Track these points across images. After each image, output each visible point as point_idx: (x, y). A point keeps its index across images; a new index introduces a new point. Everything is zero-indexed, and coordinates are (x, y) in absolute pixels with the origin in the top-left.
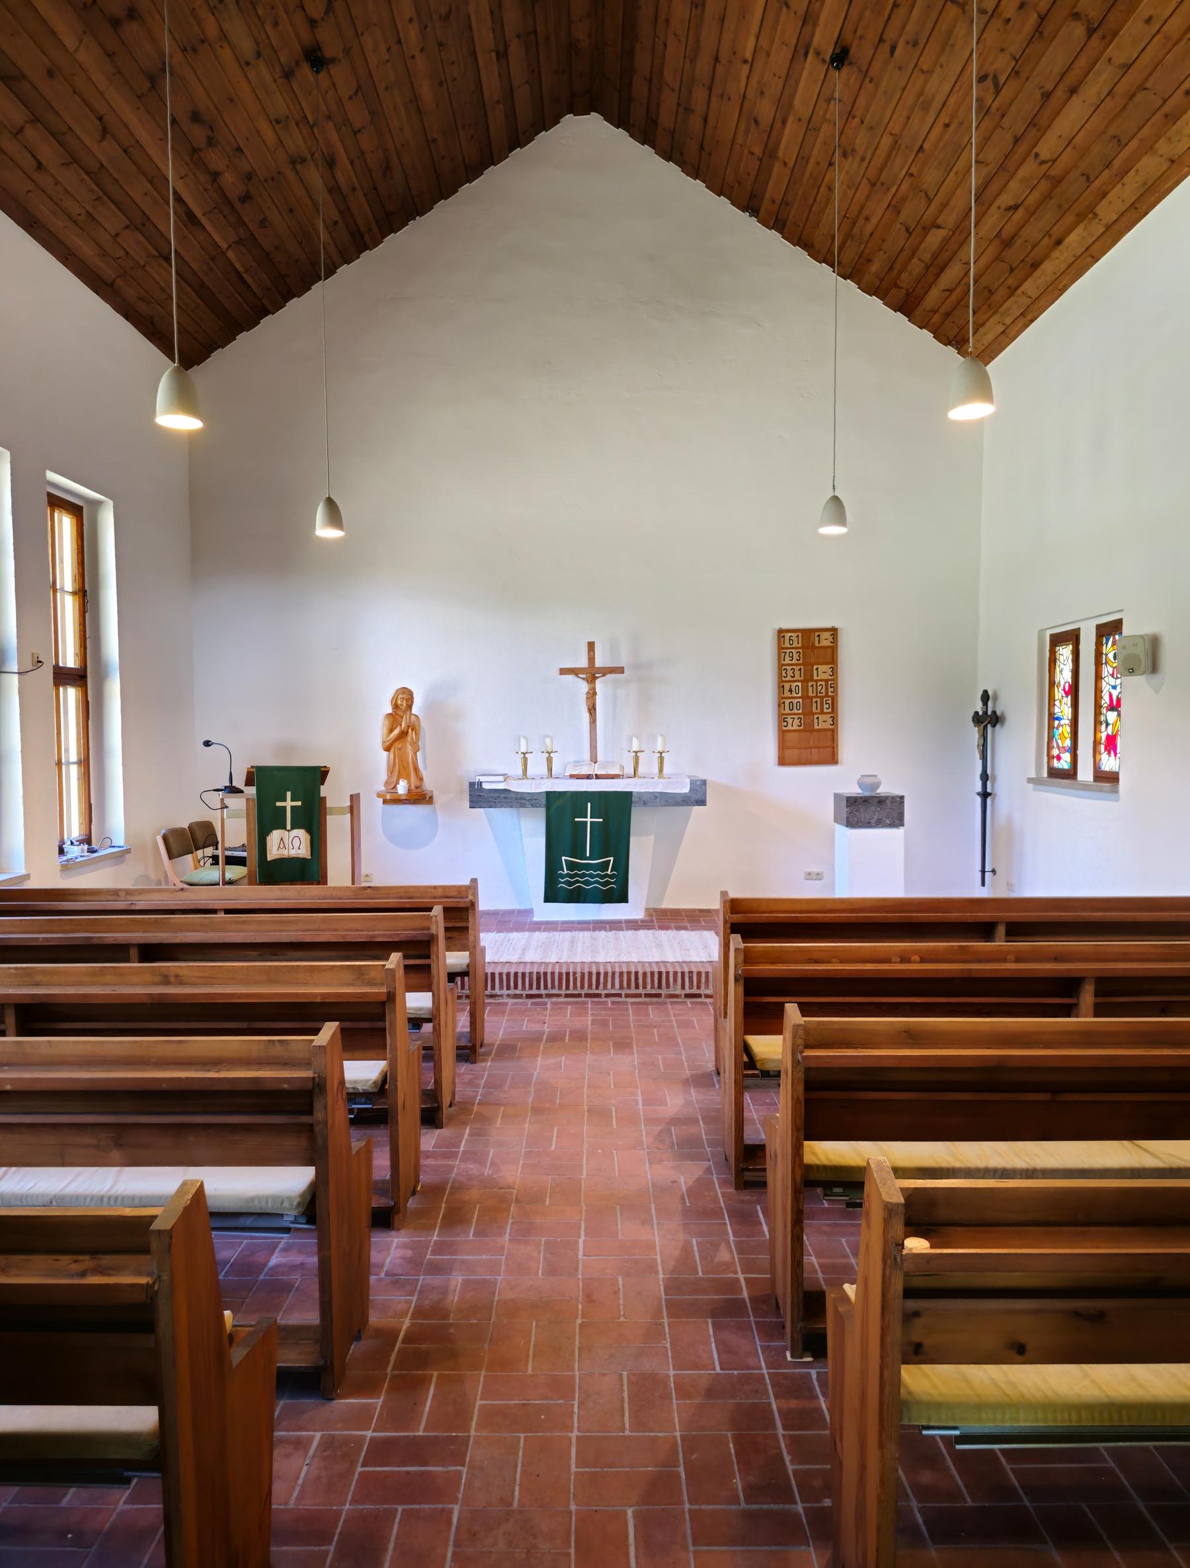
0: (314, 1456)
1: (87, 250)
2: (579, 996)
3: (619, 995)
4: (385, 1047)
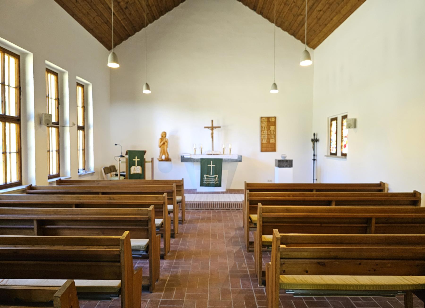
0: (149, 303)
1: (87, 22)
2: (209, 209)
3: (219, 209)
4: (162, 216)
